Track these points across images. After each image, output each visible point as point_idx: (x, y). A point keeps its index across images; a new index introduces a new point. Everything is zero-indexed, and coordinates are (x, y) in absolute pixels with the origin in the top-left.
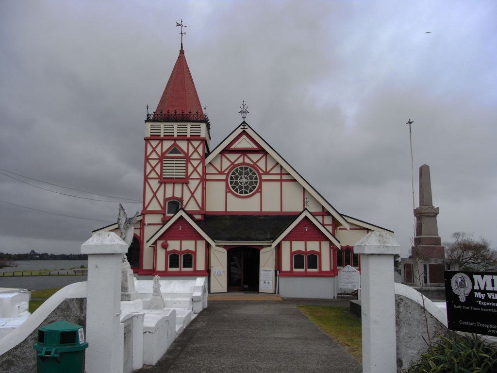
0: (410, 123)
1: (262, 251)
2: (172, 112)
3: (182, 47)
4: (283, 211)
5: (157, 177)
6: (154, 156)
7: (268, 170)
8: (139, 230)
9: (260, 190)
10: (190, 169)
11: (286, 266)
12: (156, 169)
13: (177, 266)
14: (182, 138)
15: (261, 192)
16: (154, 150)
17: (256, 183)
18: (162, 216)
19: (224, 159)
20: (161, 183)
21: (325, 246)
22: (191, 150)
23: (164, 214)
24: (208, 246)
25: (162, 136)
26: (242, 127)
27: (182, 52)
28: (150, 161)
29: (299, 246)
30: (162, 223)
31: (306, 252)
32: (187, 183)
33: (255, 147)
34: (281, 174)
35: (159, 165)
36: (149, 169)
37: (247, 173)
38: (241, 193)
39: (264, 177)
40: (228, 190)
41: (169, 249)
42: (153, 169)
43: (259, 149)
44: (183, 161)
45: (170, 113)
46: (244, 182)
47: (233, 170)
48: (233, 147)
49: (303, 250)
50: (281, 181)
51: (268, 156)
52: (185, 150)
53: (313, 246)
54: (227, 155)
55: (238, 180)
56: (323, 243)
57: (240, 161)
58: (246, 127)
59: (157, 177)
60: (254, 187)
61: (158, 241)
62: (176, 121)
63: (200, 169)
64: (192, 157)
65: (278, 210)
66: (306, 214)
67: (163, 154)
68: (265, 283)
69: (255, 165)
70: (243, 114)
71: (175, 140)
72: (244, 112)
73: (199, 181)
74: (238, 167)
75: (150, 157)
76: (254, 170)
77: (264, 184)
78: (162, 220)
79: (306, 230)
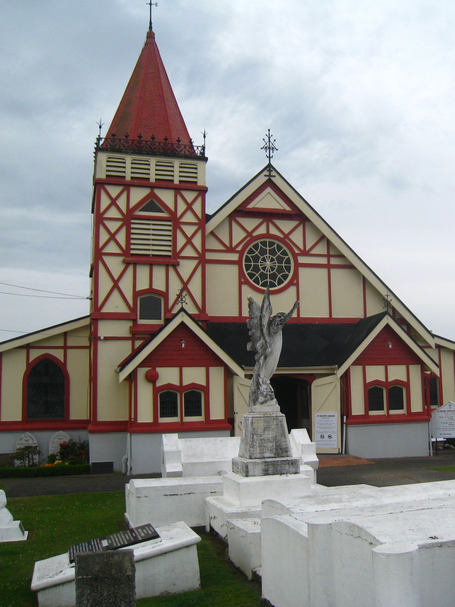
1: (315, 383)
2: (147, 137)
4: (301, 316)
6: (113, 213)
7: (307, 249)
9: (295, 282)
10: (181, 241)
13: (174, 414)
15: (297, 285)
16: (113, 202)
17: (288, 269)
18: (130, 324)
19: (235, 226)
20: (127, 264)
21: (415, 371)
22: (182, 207)
23: (135, 321)
24: (229, 374)
25: (128, 178)
27: (151, 36)
28: (107, 223)
30: (130, 336)
31: (181, 388)
32: (175, 266)
33: (288, 208)
34: (328, 256)
36: (104, 237)
37: (273, 252)
39: (302, 260)
40: (242, 281)
41: (159, 384)
42: (112, 237)
44: (168, 226)
45: (181, 143)
47: (251, 246)
48: (251, 206)
49: (383, 379)
50: (329, 266)
51: (307, 224)
52: (171, 206)
54: (240, 220)
55: (259, 264)
56: (411, 367)
57: (262, 230)
60: (285, 277)
61: (138, 368)
62: (153, 153)
63: (197, 241)
64: (183, 220)
68: (323, 437)
69: (286, 239)
70: (268, 151)
71: (152, 187)
72: (269, 148)
73: (195, 262)
74: (259, 241)
76: (285, 248)
78: (131, 332)
79: (390, 346)
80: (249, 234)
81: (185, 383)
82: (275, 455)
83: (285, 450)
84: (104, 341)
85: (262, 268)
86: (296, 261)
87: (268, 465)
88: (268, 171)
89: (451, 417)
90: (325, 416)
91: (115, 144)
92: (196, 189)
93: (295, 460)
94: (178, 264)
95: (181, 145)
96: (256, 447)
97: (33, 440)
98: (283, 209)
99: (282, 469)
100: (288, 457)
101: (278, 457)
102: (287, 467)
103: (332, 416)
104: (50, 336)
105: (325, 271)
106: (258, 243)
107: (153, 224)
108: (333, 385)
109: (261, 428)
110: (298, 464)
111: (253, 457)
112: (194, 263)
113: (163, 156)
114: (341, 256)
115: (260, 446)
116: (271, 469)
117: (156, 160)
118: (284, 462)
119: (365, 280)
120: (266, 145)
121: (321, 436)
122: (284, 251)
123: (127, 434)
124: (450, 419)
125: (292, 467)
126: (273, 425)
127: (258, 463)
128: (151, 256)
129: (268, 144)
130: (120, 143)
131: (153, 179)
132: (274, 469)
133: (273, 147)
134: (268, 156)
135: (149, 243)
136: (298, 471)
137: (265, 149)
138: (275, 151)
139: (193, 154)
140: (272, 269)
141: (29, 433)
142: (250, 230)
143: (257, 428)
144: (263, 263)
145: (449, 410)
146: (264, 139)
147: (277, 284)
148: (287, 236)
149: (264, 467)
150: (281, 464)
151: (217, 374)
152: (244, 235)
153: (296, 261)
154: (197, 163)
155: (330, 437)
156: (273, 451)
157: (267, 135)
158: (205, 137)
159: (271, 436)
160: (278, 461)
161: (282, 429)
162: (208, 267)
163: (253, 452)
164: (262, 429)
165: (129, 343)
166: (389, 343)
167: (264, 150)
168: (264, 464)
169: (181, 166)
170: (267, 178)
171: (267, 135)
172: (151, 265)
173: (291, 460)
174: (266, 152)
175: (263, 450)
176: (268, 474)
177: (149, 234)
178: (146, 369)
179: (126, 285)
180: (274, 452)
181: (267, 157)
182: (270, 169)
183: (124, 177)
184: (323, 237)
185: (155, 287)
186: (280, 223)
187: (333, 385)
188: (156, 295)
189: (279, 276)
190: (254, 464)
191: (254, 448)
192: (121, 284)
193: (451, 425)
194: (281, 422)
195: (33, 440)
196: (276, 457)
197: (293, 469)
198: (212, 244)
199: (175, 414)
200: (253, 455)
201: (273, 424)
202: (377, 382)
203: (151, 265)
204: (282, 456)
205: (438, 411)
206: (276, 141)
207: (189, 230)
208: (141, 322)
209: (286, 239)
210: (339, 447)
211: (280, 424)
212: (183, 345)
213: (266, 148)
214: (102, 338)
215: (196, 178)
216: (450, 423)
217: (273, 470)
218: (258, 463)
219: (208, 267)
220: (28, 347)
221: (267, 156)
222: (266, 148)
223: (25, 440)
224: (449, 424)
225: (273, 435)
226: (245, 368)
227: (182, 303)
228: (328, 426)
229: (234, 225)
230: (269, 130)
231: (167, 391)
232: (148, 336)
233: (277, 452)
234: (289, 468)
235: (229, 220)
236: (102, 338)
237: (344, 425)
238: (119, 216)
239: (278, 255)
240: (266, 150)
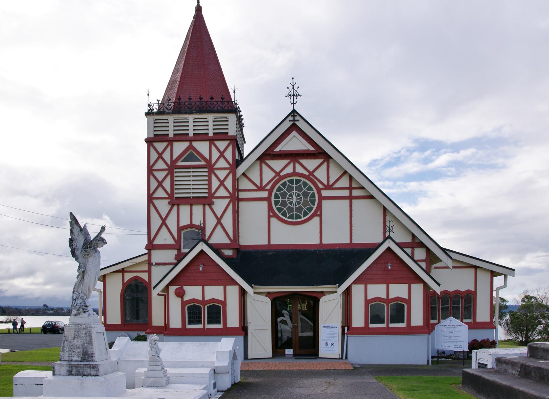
1: (322, 300)
7: (331, 183)
9: (319, 213)
10: (215, 183)
11: (358, 320)
14: (201, 137)
15: (320, 216)
20: (172, 204)
22: (216, 154)
23: (179, 250)
24: (243, 293)
28: (155, 173)
32: (210, 204)
33: (311, 148)
34: (351, 189)
35: (169, 179)
37: (299, 189)
38: (291, 217)
39: (325, 193)
40: (271, 214)
41: (186, 298)
44: (204, 172)
47: (279, 184)
48: (277, 149)
49: (200, 298)
50: (351, 198)
52: (207, 156)
55: (287, 199)
56: (413, 286)
57: (289, 170)
59: (166, 167)
60: (310, 209)
61: (237, 287)
63: (229, 183)
64: (217, 166)
67: (173, 162)
69: (311, 176)
70: (292, 98)
71: (191, 140)
72: (293, 95)
74: (286, 180)
77: (324, 202)
81: (206, 298)
82: (81, 359)
83: (90, 356)
87: (71, 367)
88: (292, 116)
89: (451, 331)
90: (329, 327)
91: (181, 106)
92: (188, 139)
93: (96, 364)
94: (213, 203)
96: (66, 351)
98: (308, 149)
99: (84, 371)
100: (93, 361)
101: (84, 361)
102: (89, 370)
103: (334, 327)
105: (348, 201)
106: (286, 181)
108: (337, 301)
109: (71, 336)
110: (98, 368)
111: (62, 360)
113: (198, 114)
114: (362, 188)
115: (70, 351)
116: (74, 370)
118: (86, 366)
119: (385, 209)
120: (290, 93)
121: (326, 344)
124: (450, 333)
125: (93, 370)
126: (83, 334)
127: (63, 365)
129: (292, 92)
130: (228, 105)
131: (171, 135)
132: (77, 370)
133: (297, 94)
136: (99, 374)
137: (289, 96)
139: (224, 109)
141: (124, 333)
142: (278, 171)
143: (68, 336)
145: (450, 324)
149: (68, 368)
150: (83, 367)
152: (273, 174)
155: (332, 344)
156: (80, 356)
157: (291, 83)
158: (148, 95)
159: (79, 343)
160: (80, 364)
161: (90, 338)
163: (62, 356)
164: (72, 337)
166: (389, 264)
167: (288, 98)
168: (68, 366)
169: (194, 120)
170: (291, 123)
171: (291, 83)
173: (92, 365)
174: (290, 99)
175: (71, 354)
176: (72, 375)
179: (172, 222)
180: (81, 357)
181: (292, 103)
182: (294, 114)
187: (337, 301)
189: (295, 213)
190: (60, 365)
191: (64, 352)
192: (167, 222)
193: (451, 339)
194: (89, 332)
196: (82, 361)
197: (93, 372)
200: (63, 358)
201: (82, 333)
202: (378, 299)
204: (87, 360)
205: (441, 326)
209: (311, 176)
210: (339, 353)
211: (89, 334)
213: (290, 95)
214: (154, 264)
216: (450, 336)
217: (76, 372)
218: (63, 365)
220: (123, 271)
221: (291, 103)
224: (449, 337)
225: (82, 342)
227: (389, 232)
228: (332, 335)
230: (293, 78)
233: (83, 357)
234: (91, 371)
235: (260, 163)
236: (154, 264)
239: (303, 190)
240: (290, 97)
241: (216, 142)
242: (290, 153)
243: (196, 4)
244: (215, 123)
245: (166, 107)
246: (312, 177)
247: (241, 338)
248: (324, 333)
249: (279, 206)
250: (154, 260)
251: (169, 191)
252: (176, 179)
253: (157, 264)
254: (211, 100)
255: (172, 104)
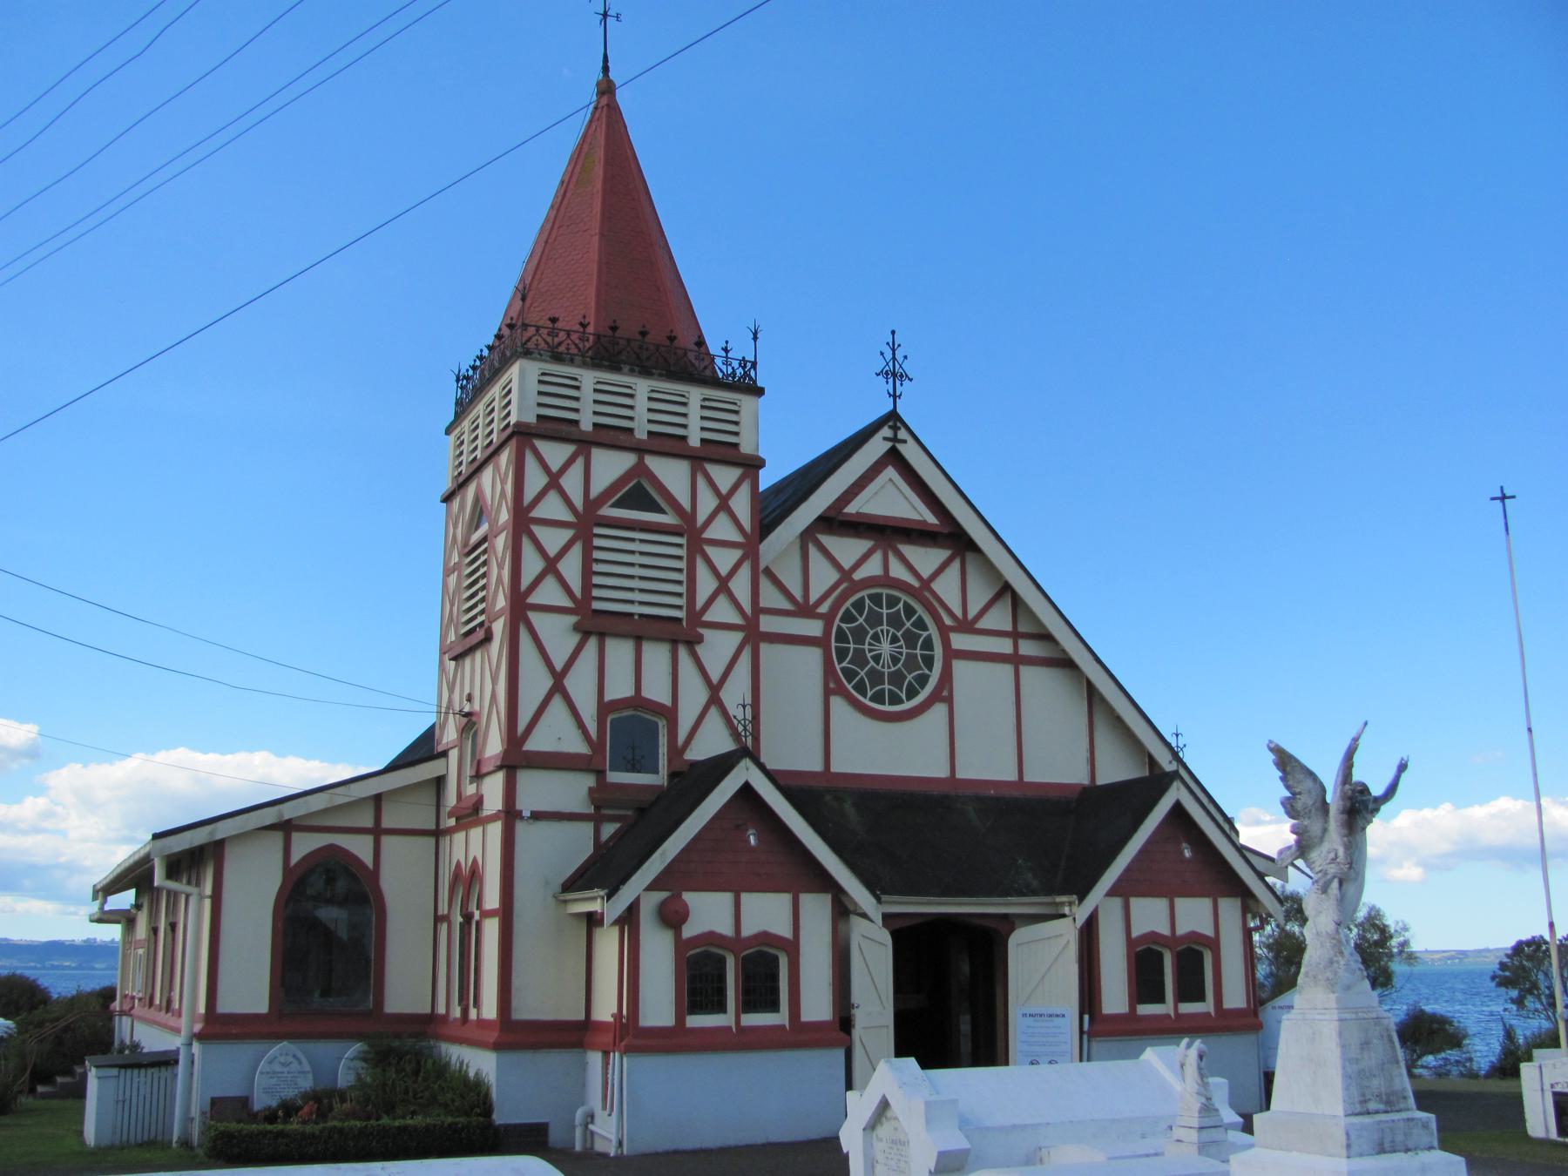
0: (1503, 498)
3: (606, 69)
4: (960, 775)
5: (568, 603)
6: (552, 508)
7: (971, 615)
8: (433, 827)
9: (945, 693)
10: (706, 584)
11: (1115, 996)
12: (733, 585)
14: (671, 445)
15: (949, 701)
16: (554, 482)
17: (929, 661)
22: (707, 504)
23: (600, 774)
24: (843, 910)
26: (886, 431)
27: (607, 89)
29: (1150, 915)
30: (592, 810)
32: (693, 642)
33: (931, 519)
34: (1015, 635)
36: (532, 565)
37: (895, 621)
38: (878, 698)
39: (959, 641)
40: (832, 685)
41: (689, 931)
42: (551, 566)
43: (946, 531)
46: (886, 657)
48: (851, 509)
49: (1165, 930)
50: (1016, 660)
52: (685, 502)
53: (1194, 915)
55: (866, 647)
56: (807, 900)
57: (872, 568)
58: (902, 434)
59: (568, 603)
60: (923, 680)
63: (741, 586)
65: (1010, 775)
66: (744, 773)
67: (592, 504)
69: (923, 590)
70: (891, 381)
71: (640, 450)
72: (894, 375)
74: (864, 593)
75: (536, 513)
76: (920, 611)
77: (959, 666)
79: (752, 840)
80: (846, 575)
81: (748, 930)
84: (531, 821)
85: (873, 657)
86: (946, 643)
88: (890, 427)
94: (700, 639)
95: (620, 338)
97: (300, 1063)
98: (921, 519)
103: (1057, 1016)
104: (353, 799)
105: (1006, 670)
107: (642, 541)
112: (736, 638)
114: (1046, 637)
117: (702, 394)
120: (887, 368)
122: (920, 619)
123: (585, 1052)
128: (636, 617)
129: (891, 364)
131: (586, 425)
133: (902, 374)
134: (891, 392)
135: (632, 586)
138: (906, 382)
140: (895, 660)
141: (291, 1046)
142: (847, 565)
144: (875, 646)
146: (882, 354)
147: (904, 698)
148: (926, 583)
151: (816, 908)
152: (834, 576)
153: (946, 643)
154: (740, 400)
157: (888, 344)
158: (755, 338)
162: (765, 649)
165: (587, 829)
166: (751, 831)
167: (881, 379)
170: (889, 445)
171: (888, 344)
172: (639, 639)
174: (887, 382)
177: (632, 565)
178: (663, 895)
181: (890, 395)
183: (684, 438)
184: (1006, 589)
185: (646, 693)
186: (910, 551)
187: (1063, 941)
188: (645, 713)
189: (887, 686)
192: (570, 683)
195: (300, 1063)
198: (770, 597)
199: (720, 1007)
202: (1153, 936)
203: (639, 639)
205: (1274, 1008)
206: (908, 358)
207: (724, 559)
208: (615, 777)
209: (923, 590)
212: (752, 840)
213: (887, 373)
214: (526, 814)
215: (736, 434)
219: (765, 649)
220: (286, 828)
221: (889, 393)
222: (887, 373)
223: (280, 1063)
226: (883, 899)
229: (813, 552)
230: (893, 332)
231: (705, 951)
232: (630, 813)
236: (526, 814)
237: (1085, 1037)
238: (567, 516)
241: (541, 445)
242: (881, 522)
243: (598, 75)
244: (573, 404)
245: (544, 340)
246: (927, 594)
247: (840, 1054)
248: (1024, 1033)
249: (848, 663)
250: (525, 805)
251: (577, 591)
252: (597, 555)
253: (537, 816)
254: (696, 348)
255: (591, 338)
